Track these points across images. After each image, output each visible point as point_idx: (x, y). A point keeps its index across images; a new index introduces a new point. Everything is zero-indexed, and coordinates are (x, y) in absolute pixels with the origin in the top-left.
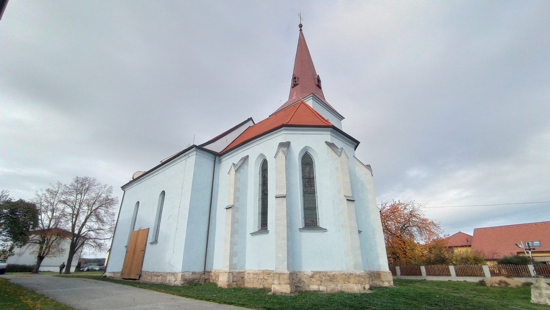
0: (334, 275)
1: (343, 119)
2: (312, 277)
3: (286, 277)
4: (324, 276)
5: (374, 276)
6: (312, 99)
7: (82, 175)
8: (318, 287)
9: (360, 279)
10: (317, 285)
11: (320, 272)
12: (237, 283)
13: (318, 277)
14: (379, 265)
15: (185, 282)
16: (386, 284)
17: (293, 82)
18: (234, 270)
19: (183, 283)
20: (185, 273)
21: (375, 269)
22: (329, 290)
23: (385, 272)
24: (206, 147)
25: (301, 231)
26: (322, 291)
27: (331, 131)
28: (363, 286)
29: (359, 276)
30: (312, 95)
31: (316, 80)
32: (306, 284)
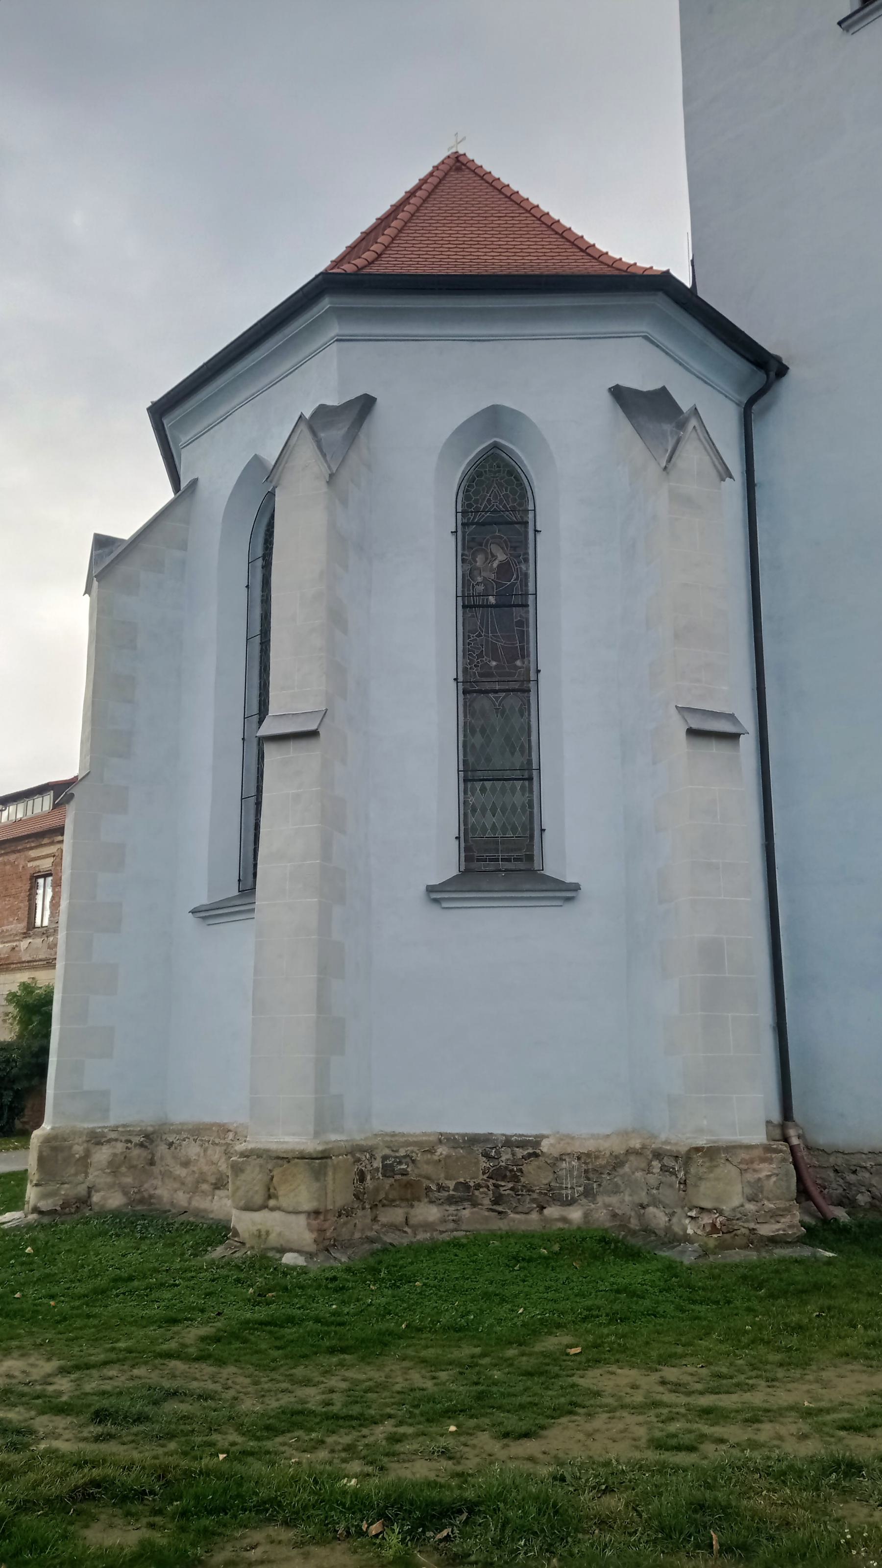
27: (340, 313)
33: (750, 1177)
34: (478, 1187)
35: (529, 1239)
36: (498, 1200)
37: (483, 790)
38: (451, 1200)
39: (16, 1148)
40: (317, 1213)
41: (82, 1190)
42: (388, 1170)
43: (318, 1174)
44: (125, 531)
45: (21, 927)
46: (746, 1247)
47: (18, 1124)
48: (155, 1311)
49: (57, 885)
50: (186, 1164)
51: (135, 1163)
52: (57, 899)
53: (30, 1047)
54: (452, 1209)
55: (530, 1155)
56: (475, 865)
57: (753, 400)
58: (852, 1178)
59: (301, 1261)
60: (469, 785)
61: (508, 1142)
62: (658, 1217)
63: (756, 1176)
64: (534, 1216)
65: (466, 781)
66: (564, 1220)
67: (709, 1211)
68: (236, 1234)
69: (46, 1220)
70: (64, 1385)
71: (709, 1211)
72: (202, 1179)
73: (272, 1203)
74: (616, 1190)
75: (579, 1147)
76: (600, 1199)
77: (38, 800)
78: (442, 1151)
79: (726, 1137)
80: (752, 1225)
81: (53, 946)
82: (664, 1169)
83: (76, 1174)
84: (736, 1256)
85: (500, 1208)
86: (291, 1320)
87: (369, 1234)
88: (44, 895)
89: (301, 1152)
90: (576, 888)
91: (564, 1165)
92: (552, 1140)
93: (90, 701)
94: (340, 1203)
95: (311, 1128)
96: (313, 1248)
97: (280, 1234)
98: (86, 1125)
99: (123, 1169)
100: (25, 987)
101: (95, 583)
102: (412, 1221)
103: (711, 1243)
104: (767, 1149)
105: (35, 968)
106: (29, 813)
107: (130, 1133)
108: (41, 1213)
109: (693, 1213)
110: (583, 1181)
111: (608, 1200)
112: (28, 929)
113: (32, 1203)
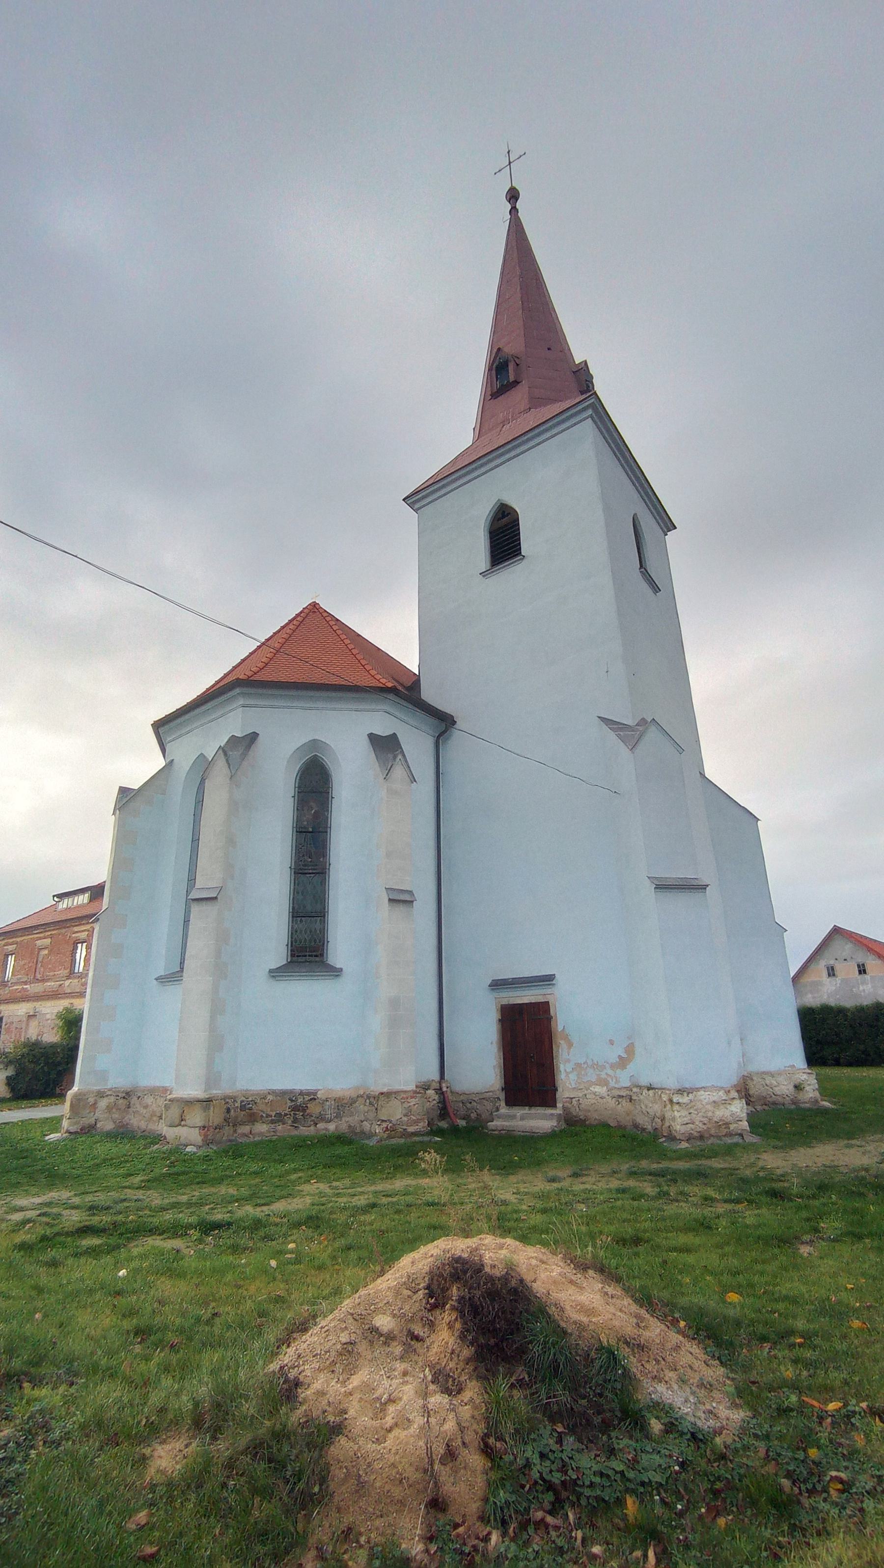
6: (591, 416)
27: (243, 695)
33: (406, 1105)
34: (286, 1115)
35: (304, 1139)
36: (295, 1120)
37: (301, 921)
38: (272, 1122)
39: (56, 1104)
40: (204, 1127)
41: (92, 1121)
42: (243, 1108)
43: (206, 1109)
44: (135, 784)
45: (66, 972)
46: (401, 1137)
47: (58, 1091)
48: (121, 1171)
49: (89, 948)
50: (146, 1107)
51: (120, 1107)
52: (88, 956)
53: (68, 1045)
54: (272, 1126)
55: (311, 1099)
56: (295, 959)
57: (438, 737)
58: (469, 1105)
59: (195, 1150)
60: (295, 919)
61: (301, 1093)
62: (366, 1126)
63: (409, 1104)
64: (312, 1128)
65: (293, 917)
66: (326, 1129)
67: (386, 1121)
68: (165, 1138)
69: (72, 1137)
70: (77, 1200)
71: (386, 1121)
72: (153, 1114)
73: (183, 1123)
74: (352, 1115)
75: (334, 1095)
76: (343, 1119)
77: (81, 897)
78: (270, 1097)
79: (397, 1087)
80: (405, 1127)
81: (85, 984)
82: (371, 1103)
83: (90, 1112)
84: (394, 1141)
85: (296, 1125)
86: (184, 1173)
87: (231, 1138)
88: (81, 952)
89: (198, 1098)
90: (341, 970)
91: (328, 1103)
92: (323, 1092)
93: (111, 871)
94: (215, 1124)
95: (203, 1086)
96: (200, 1144)
97: (186, 1138)
98: (95, 1088)
99: (114, 1110)
100: (66, 1009)
101: (118, 812)
102: (253, 1132)
103: (385, 1136)
104: (415, 1092)
105: (73, 997)
106: (75, 904)
107: (119, 1092)
108: (70, 1133)
109: (379, 1123)
110: (336, 1110)
111: (347, 1119)
112: (70, 974)
113: (65, 1128)
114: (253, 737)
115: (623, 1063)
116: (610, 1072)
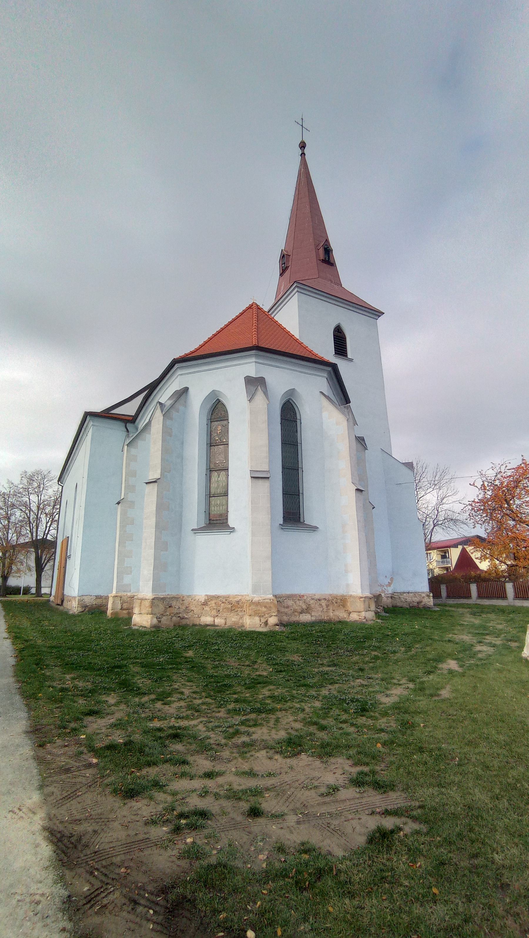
0: (238, 602)
1: (379, 316)
2: (205, 604)
3: (147, 603)
4: (223, 602)
5: (336, 603)
6: (297, 291)
7: (30, 470)
8: (212, 619)
9: (259, 608)
10: (211, 616)
11: (218, 597)
12: (130, 611)
13: (214, 605)
14: (348, 585)
15: (85, 610)
16: (354, 617)
17: (281, 265)
18: (125, 594)
19: (81, 611)
20: (84, 597)
21: (340, 591)
22: (229, 623)
23: (354, 597)
24: (116, 411)
25: (282, 528)
26: (218, 626)
27: (256, 356)
28: (263, 620)
29: (258, 604)
30: (295, 285)
31: (321, 251)
32: (196, 615)
114: (186, 390)
115: (389, 584)
116: (386, 588)
